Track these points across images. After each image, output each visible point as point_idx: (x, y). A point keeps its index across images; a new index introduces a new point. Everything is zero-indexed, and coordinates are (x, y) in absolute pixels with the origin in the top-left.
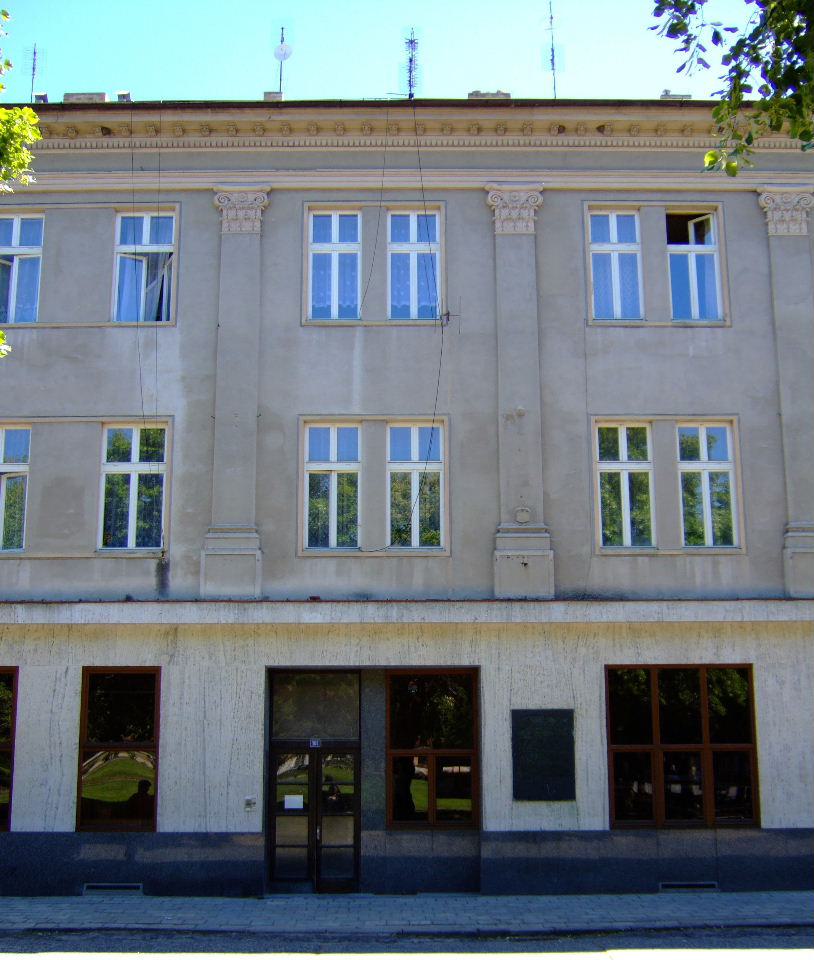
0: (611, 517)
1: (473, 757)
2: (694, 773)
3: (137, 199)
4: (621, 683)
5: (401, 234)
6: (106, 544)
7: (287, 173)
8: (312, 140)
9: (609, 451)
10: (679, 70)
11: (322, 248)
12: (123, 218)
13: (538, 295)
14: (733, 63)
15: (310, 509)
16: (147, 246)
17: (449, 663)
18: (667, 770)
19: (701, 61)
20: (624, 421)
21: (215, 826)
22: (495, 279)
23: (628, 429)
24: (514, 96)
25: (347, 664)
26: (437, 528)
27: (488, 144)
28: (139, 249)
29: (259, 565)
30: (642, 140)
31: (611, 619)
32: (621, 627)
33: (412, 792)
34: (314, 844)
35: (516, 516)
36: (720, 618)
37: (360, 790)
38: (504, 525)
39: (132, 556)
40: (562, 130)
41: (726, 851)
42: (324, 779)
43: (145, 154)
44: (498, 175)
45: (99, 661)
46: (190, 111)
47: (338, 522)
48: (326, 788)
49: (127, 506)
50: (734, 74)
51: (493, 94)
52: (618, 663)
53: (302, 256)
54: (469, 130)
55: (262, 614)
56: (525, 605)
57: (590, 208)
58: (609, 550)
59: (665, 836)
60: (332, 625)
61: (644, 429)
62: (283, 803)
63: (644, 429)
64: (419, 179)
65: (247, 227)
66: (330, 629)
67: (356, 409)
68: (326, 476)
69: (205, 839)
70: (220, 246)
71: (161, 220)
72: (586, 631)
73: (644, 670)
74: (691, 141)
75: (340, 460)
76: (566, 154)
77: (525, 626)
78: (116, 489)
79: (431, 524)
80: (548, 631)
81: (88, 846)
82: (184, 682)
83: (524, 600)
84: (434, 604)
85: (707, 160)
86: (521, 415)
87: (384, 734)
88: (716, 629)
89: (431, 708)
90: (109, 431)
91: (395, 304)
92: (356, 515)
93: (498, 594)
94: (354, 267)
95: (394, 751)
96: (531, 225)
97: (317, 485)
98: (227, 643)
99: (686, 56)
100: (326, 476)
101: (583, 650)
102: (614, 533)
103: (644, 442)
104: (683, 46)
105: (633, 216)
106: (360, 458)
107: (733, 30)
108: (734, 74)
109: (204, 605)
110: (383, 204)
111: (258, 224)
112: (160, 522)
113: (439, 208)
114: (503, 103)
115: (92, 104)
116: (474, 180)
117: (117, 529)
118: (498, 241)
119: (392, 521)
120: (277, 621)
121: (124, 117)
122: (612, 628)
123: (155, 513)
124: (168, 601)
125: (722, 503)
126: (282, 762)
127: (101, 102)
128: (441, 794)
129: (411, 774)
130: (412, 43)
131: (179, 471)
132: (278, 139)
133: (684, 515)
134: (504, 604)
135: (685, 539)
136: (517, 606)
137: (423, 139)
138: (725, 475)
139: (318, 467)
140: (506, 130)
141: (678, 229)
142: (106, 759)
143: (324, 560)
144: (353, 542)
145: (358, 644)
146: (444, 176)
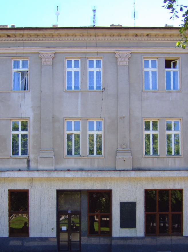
0: (147, 147)
1: (110, 216)
2: (167, 220)
3: (18, 55)
4: (148, 193)
5: (91, 65)
6: (13, 154)
7: (59, 48)
8: (66, 38)
9: (147, 128)
10: (170, 18)
11: (69, 70)
12: (14, 61)
13: (129, 83)
14: (186, 16)
15: (67, 144)
16: (21, 69)
17: (104, 189)
18: (160, 219)
19: (176, 16)
20: (151, 119)
21: (44, 235)
22: (117, 78)
23: (153, 121)
24: (123, 26)
25: (77, 189)
26: (101, 150)
27: (110, 39)
28: (19, 70)
29: (54, 160)
30: (159, 38)
31: (146, 176)
32: (149, 179)
33: (94, 225)
34: (69, 240)
35: (122, 146)
36: (175, 176)
37: (81, 225)
38: (119, 149)
39: (20, 158)
40: (136, 35)
41: (174, 243)
42: (72, 222)
43: (20, 42)
44: (119, 49)
45: (13, 188)
46: (32, 30)
47: (75, 148)
48: (72, 224)
49: (18, 143)
50: (186, 20)
51: (117, 25)
52: (148, 189)
53: (64, 72)
54: (110, 36)
55: (55, 175)
56: (124, 172)
57: (144, 58)
58: (147, 156)
59: (158, 238)
60: (73, 178)
61: (157, 121)
62: (61, 229)
63: (157, 121)
64: (96, 50)
65: (49, 63)
66: (73, 179)
67: (79, 116)
68: (71, 135)
69: (42, 239)
70: (41, 69)
71: (25, 62)
72: (139, 180)
73: (155, 191)
74: (173, 39)
75: (75, 130)
76: (137, 43)
77: (124, 178)
78: (15, 138)
79: (99, 149)
80: (130, 179)
81: (12, 241)
82: (35, 194)
83: (124, 170)
84: (100, 172)
85: (177, 44)
86: (124, 117)
87: (87, 209)
88: (174, 179)
89: (99, 200)
90: (13, 122)
91: (90, 85)
92: (79, 146)
93: (117, 168)
94: (78, 75)
95: (90, 214)
96: (128, 63)
97: (69, 137)
98: (46, 183)
99: (172, 14)
100: (71, 135)
101: (139, 185)
102: (148, 151)
103: (157, 125)
104: (172, 11)
105: (156, 60)
106: (80, 130)
107: (186, 7)
108: (186, 20)
109: (40, 172)
110: (86, 57)
111: (52, 63)
112: (27, 148)
113: (102, 58)
114: (120, 28)
115: (4, 28)
116: (112, 50)
117: (16, 150)
118: (118, 67)
119: (89, 148)
120: (59, 177)
121: (13, 32)
122: (147, 178)
123: (26, 146)
124: (30, 171)
125: (177, 143)
126: (61, 217)
127: (6, 27)
128: (102, 226)
129: (94, 221)
130: (94, 11)
131: (32, 134)
132: (57, 38)
133: (167, 146)
134: (119, 172)
135: (167, 153)
136: (122, 172)
137: (97, 38)
138: (178, 134)
139: (69, 132)
140: (121, 36)
141: (168, 64)
142: (16, 216)
143: (71, 159)
144: (79, 154)
145: (80, 183)
146: (103, 49)
